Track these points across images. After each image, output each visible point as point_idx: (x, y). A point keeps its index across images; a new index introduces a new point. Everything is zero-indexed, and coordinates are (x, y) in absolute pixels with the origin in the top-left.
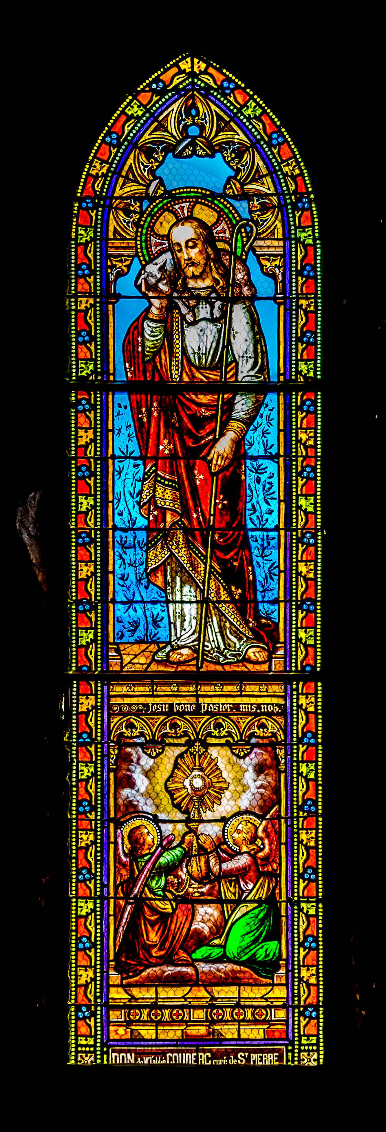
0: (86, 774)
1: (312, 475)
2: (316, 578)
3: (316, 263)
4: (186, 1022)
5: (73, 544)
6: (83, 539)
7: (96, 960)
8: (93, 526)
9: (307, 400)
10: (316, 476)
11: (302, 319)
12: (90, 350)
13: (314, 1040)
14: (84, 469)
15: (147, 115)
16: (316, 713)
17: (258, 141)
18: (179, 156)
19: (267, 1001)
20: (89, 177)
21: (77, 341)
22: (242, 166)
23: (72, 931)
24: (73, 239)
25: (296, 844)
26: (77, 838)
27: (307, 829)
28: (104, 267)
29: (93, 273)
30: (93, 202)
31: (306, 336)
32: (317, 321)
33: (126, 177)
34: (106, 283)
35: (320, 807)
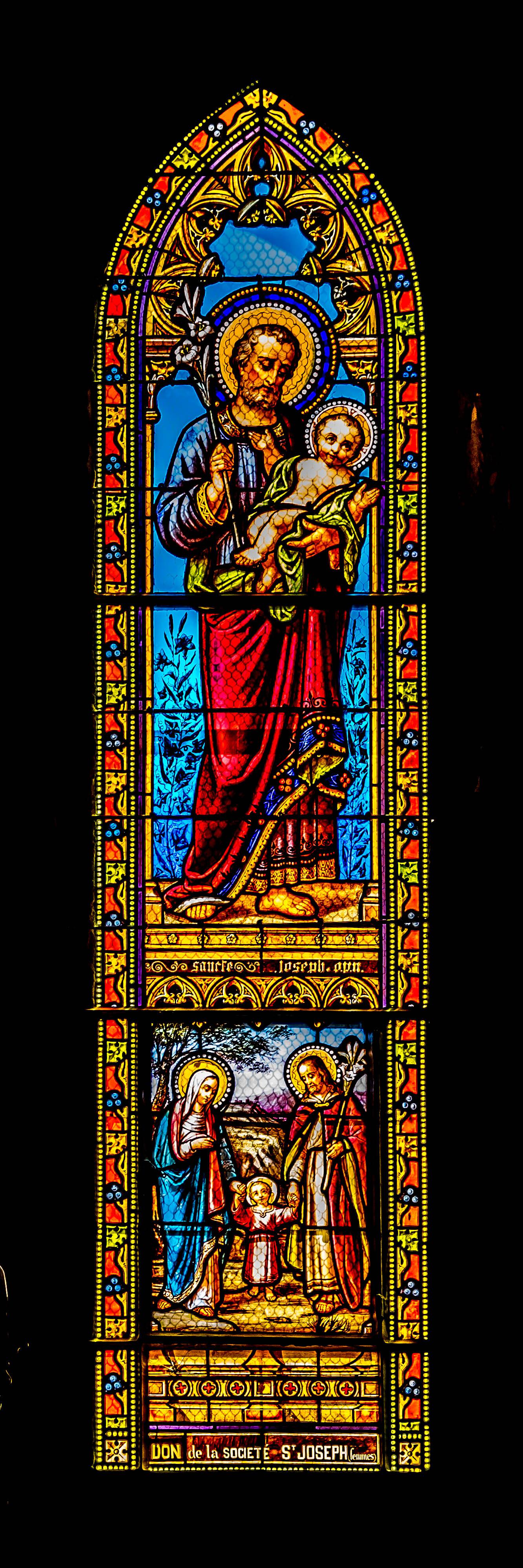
2: (420, 514)
3: (420, 640)
4: (248, 1398)
5: (100, 1199)
6: (113, 375)
7: (128, 852)
10: (420, 556)
11: (403, 895)
12: (120, 393)
16: (420, 794)
18: (244, 224)
19: (357, 1370)
20: (123, 251)
21: (104, 559)
22: (326, 237)
26: (104, 503)
28: (140, 372)
29: (125, 379)
30: (127, 283)
35: (425, 1290)
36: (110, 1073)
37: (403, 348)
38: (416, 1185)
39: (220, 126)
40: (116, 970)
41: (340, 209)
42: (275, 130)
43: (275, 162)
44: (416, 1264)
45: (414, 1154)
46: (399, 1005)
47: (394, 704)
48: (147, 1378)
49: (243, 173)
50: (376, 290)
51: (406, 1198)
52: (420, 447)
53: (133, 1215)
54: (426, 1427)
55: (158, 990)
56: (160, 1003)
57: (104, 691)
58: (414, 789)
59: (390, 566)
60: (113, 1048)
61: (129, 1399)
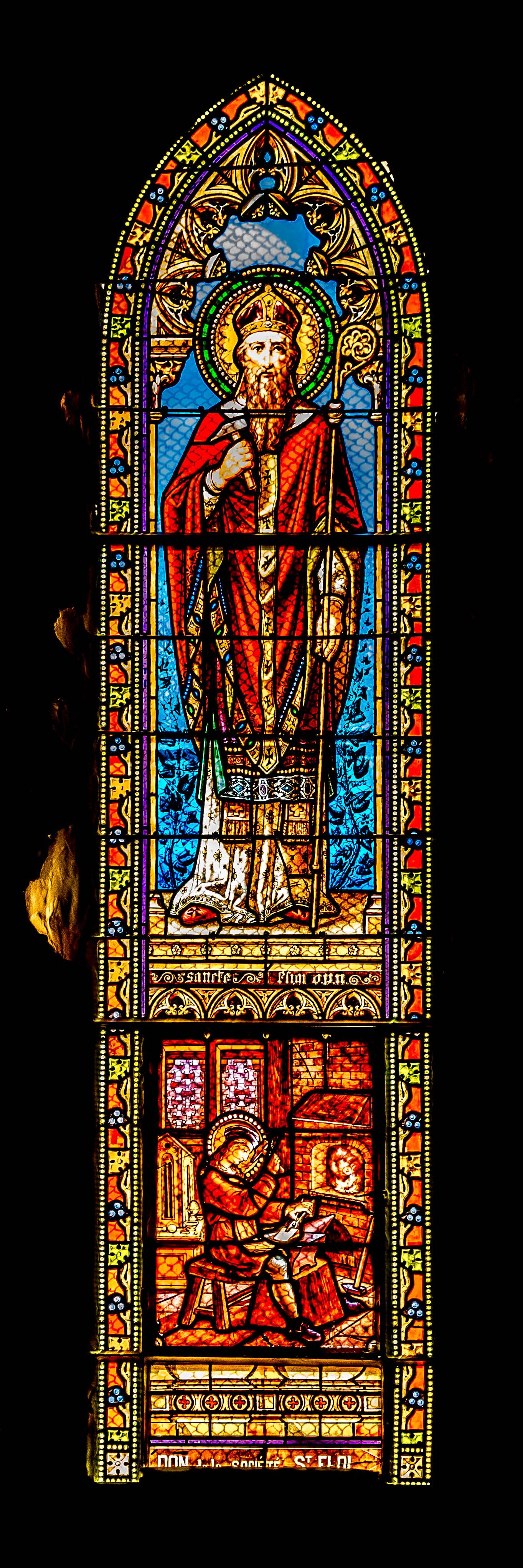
0: (119, 701)
8: (129, 730)
9: (412, 646)
14: (117, 462)
15: (203, 163)
16: (423, 988)
18: (247, 218)
20: (127, 248)
22: (332, 232)
23: (100, 1323)
24: (104, 704)
25: (395, 797)
26: (107, 1065)
27: (410, 687)
31: (410, 561)
32: (425, 816)
35: (430, 1400)
36: (112, 1091)
37: (406, 1095)
38: (422, 1388)
39: (224, 119)
40: (119, 1076)
41: (347, 205)
43: (280, 155)
45: (418, 982)
46: (402, 1017)
48: (150, 1394)
52: (425, 916)
53: (135, 1228)
54: (428, 1231)
55: (161, 1004)
56: (163, 1015)
57: (108, 697)
58: (417, 1173)
60: (116, 601)
61: (133, 482)
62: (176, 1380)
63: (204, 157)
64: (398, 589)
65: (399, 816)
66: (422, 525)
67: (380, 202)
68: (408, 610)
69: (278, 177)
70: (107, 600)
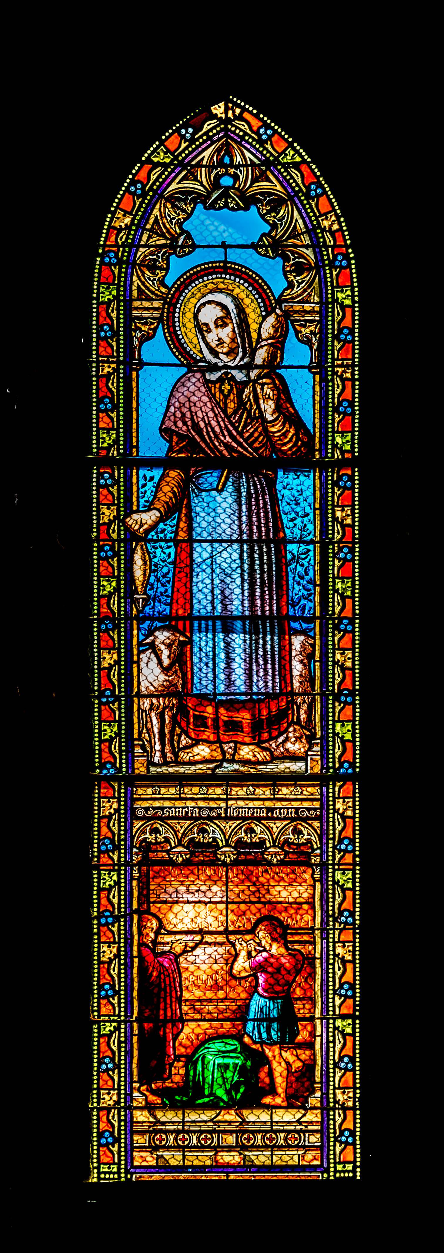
1: (349, 556)
12: (112, 419)
13: (350, 1167)
17: (296, 193)
18: (212, 207)
26: (99, 806)
28: (128, 331)
31: (342, 988)
33: (152, 230)
34: (129, 349)
35: (358, 918)
40: (110, 736)
42: (238, 135)
44: (351, 825)
47: (334, 925)
49: (210, 167)
50: (319, 267)
51: (342, 1065)
59: (331, 743)
62: (158, 1122)
63: (176, 158)
64: (334, 1159)
65: (333, 678)
66: (352, 451)
67: (318, 196)
68: (342, 1100)
69: (236, 177)
70: (99, 947)
